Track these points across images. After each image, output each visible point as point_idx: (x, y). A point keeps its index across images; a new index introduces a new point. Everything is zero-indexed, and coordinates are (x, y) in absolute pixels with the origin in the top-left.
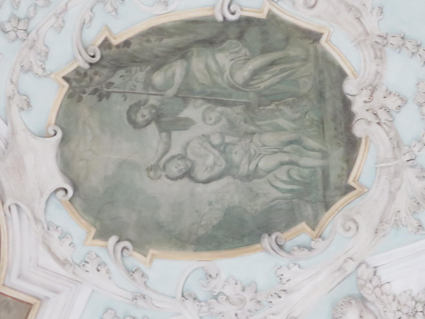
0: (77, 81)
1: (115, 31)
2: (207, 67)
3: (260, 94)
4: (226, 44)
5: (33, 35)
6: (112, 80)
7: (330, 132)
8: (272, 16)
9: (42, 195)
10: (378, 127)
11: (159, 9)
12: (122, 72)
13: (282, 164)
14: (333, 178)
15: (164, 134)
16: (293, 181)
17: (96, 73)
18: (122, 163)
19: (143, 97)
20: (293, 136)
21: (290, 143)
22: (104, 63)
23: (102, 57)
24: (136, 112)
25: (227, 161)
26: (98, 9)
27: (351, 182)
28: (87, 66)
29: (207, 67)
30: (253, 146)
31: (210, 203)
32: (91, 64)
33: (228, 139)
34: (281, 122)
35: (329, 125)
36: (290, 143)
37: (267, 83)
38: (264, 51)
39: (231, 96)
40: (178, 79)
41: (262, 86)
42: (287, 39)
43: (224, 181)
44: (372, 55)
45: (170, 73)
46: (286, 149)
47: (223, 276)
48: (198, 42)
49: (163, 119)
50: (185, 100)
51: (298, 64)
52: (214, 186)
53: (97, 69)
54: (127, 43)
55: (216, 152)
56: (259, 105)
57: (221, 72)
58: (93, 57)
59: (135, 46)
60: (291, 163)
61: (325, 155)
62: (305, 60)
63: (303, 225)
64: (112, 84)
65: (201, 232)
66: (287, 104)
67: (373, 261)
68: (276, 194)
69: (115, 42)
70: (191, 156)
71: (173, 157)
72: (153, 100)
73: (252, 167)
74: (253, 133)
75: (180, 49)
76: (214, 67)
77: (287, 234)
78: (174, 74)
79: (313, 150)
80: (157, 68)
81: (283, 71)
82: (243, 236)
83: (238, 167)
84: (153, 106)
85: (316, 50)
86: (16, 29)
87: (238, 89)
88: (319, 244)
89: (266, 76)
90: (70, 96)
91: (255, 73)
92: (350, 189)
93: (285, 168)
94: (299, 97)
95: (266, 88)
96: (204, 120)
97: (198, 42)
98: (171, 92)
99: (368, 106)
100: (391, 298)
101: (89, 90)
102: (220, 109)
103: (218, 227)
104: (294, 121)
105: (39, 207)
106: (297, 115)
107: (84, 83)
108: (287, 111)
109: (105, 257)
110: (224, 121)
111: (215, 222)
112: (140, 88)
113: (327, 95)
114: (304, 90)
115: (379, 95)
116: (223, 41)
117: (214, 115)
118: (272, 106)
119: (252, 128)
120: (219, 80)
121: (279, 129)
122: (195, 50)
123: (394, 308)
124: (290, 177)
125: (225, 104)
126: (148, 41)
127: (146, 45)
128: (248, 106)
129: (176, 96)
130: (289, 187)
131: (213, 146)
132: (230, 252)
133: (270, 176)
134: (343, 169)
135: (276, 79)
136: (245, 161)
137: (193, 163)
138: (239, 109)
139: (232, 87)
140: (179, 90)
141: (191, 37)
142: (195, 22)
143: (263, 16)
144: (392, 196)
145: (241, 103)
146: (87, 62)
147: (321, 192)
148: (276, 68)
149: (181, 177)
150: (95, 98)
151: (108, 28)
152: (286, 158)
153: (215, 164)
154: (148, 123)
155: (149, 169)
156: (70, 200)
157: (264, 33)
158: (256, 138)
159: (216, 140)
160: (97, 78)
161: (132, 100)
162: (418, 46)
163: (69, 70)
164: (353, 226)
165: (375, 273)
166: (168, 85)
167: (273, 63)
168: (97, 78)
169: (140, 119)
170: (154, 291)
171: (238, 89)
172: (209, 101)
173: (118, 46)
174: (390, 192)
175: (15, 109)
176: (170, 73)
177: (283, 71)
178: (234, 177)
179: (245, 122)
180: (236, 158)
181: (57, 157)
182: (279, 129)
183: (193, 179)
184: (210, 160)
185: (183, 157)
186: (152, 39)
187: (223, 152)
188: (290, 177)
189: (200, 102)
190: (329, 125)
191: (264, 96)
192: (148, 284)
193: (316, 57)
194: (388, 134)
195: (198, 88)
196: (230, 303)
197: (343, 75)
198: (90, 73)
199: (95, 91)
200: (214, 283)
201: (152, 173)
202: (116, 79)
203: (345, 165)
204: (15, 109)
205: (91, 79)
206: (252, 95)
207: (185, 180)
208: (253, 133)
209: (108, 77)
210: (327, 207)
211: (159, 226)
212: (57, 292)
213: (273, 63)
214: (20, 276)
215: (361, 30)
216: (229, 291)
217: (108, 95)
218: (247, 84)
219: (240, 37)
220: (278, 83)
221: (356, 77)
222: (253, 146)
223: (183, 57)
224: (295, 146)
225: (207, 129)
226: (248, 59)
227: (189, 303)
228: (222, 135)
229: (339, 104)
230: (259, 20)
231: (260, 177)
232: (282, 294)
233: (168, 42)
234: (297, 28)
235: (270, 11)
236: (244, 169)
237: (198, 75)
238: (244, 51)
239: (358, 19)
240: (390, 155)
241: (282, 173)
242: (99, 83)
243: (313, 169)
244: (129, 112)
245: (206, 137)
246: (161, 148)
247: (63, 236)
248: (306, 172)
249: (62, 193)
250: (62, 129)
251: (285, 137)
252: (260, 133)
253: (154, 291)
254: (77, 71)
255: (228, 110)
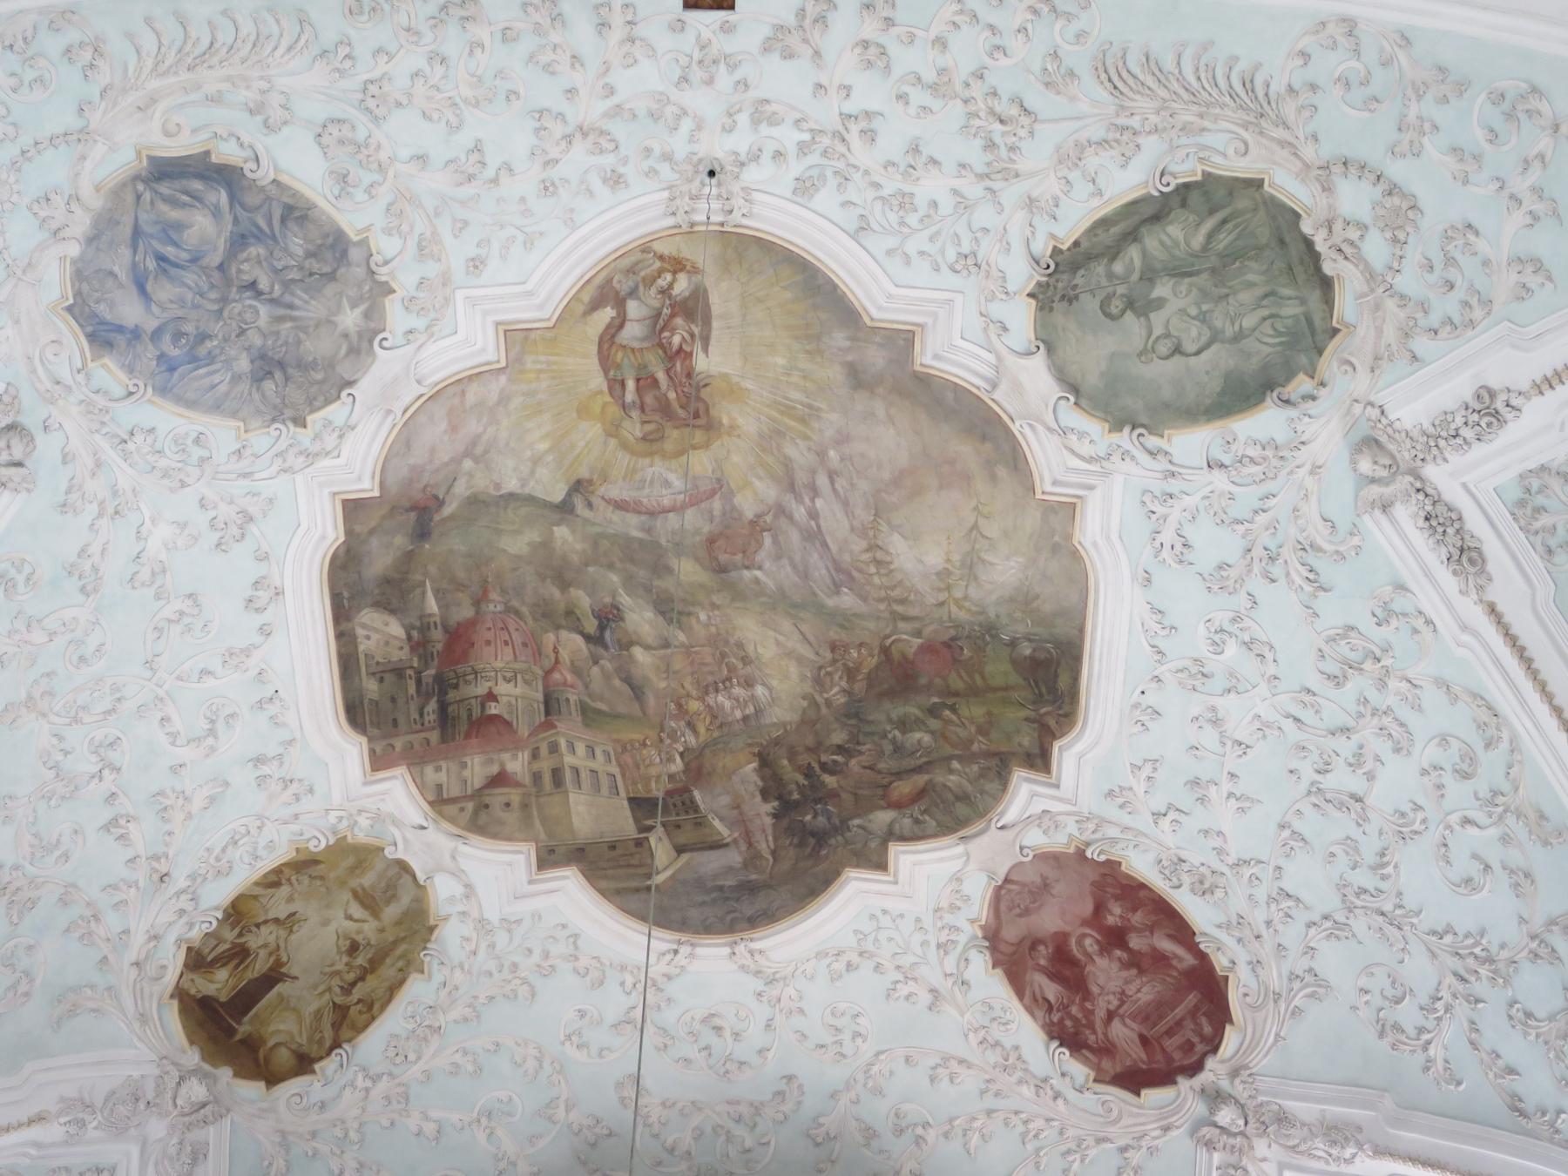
0: (1043, 293)
1: (1060, 234)
2: (1162, 243)
3: (1222, 256)
4: (1172, 216)
5: (984, 266)
6: (1075, 282)
7: (1301, 277)
8: (1206, 175)
9: (1047, 406)
10: (1345, 262)
11: (1096, 202)
12: (1082, 272)
13: (1264, 319)
14: (1318, 322)
15: (1142, 319)
16: (1279, 334)
17: (1057, 281)
18: (1113, 357)
19: (1110, 290)
20: (1266, 289)
21: (1266, 296)
22: (1061, 268)
23: (1057, 265)
24: (1109, 305)
25: (1210, 328)
26: (1037, 221)
27: (1334, 324)
28: (1044, 279)
29: (1162, 243)
30: (1231, 308)
31: (1207, 373)
32: (1049, 275)
33: (1205, 307)
34: (1250, 277)
35: (1298, 270)
36: (1266, 296)
37: (1225, 242)
38: (1212, 212)
39: (1193, 265)
40: (1137, 262)
41: (1221, 246)
42: (1231, 194)
43: (1214, 347)
44: (1319, 188)
45: (1127, 260)
46: (1264, 302)
47: (1242, 438)
48: (1144, 222)
49: (1137, 305)
50: (1151, 281)
51: (1248, 216)
52: (1205, 356)
53: (1057, 276)
54: (1076, 244)
55: (1196, 322)
56: (1224, 267)
57: (1177, 244)
58: (1048, 267)
59: (1085, 244)
60: (1272, 316)
61: (1303, 301)
62: (1255, 210)
63: (1301, 377)
64: (1076, 286)
65: (1208, 402)
66: (1249, 259)
67: (1378, 399)
68: (1268, 350)
69: (1064, 247)
70: (1174, 333)
71: (1158, 338)
72: (1121, 290)
73: (1237, 327)
74: (1227, 295)
75: (1130, 233)
76: (1168, 242)
77: (1289, 388)
78: (1132, 259)
79: (1290, 298)
80: (1113, 259)
81: (1236, 226)
82: (1248, 398)
83: (1223, 332)
84: (1123, 295)
85: (1262, 196)
86: (966, 267)
87: (1197, 256)
88: (1323, 392)
89: (1222, 236)
90: (1040, 308)
91: (1210, 236)
92: (1335, 331)
93: (1268, 322)
94: (1260, 249)
95: (1225, 248)
96: (1175, 295)
97: (1144, 222)
98: (1135, 277)
99: (1329, 243)
100: (1403, 434)
101: (1057, 298)
102: (1187, 280)
103: (1223, 393)
104: (1264, 273)
105: (1049, 418)
106: (1264, 267)
107: (1050, 293)
108: (1252, 264)
109: (1127, 445)
110: (1195, 291)
111: (1218, 389)
112: (1104, 282)
113: (1287, 239)
114: (1264, 241)
115: (1338, 227)
116: (1168, 214)
117: (1183, 288)
118: (1237, 264)
119: (1226, 291)
120: (1177, 253)
121: (1251, 285)
122: (1144, 230)
123: (1409, 446)
124: (1275, 330)
125: (1190, 274)
126: (1096, 235)
127: (1094, 240)
128: (1213, 271)
129: (1141, 279)
130: (1277, 340)
131: (1193, 318)
132: (1240, 416)
133: (1257, 332)
134: (1324, 311)
135: (1231, 238)
136: (1228, 323)
137: (1178, 338)
138: (1205, 276)
139: (1192, 255)
140: (1143, 273)
141: (1136, 219)
142: (1134, 203)
143: (1199, 177)
144: (1379, 331)
145: (1206, 270)
146: (1044, 275)
147: (1310, 339)
148: (1229, 226)
149: (1172, 355)
150: (1065, 304)
151: (1053, 236)
152: (1266, 312)
153: (1200, 334)
154: (1123, 312)
155: (1140, 355)
156: (1075, 404)
157: (1206, 193)
158: (1231, 299)
159: (1193, 311)
160: (1060, 285)
161: (1101, 295)
162: (1363, 167)
163: (1030, 288)
164: (1349, 369)
165: (1383, 413)
166: (1130, 269)
167: (1224, 222)
168: (1060, 285)
169: (1114, 311)
170: (1182, 466)
171: (1197, 256)
172: (1174, 276)
173: (1069, 249)
174: (1376, 327)
175: (994, 338)
176: (1127, 260)
177: (1236, 226)
178: (1223, 342)
179: (1216, 286)
180: (1218, 324)
181: (1050, 369)
182: (1251, 285)
183: (1182, 353)
184: (1194, 332)
185: (1167, 335)
186: (1099, 231)
187: (1203, 321)
188: (1275, 330)
189: (1167, 278)
190: (1298, 270)
191: (1227, 256)
192: (1175, 461)
193: (1265, 203)
194: (1356, 266)
195: (1158, 266)
196: (334, 1099)
197: (1298, 216)
198: (1052, 281)
199: (1063, 297)
200: (1234, 447)
201: (1143, 358)
202: (1079, 280)
203: (1325, 307)
204: (994, 338)
205: (1055, 288)
206: (1213, 258)
207: (1177, 358)
208: (1227, 295)
209: (1070, 281)
210: (1320, 352)
211: (1167, 406)
212: (1091, 488)
213: (1224, 222)
214: (1055, 483)
215: (1299, 164)
216: (1251, 452)
217: (1077, 297)
218: (1206, 248)
219: (1184, 204)
220: (1235, 240)
221: (1309, 215)
222: (1231, 308)
223: (1135, 240)
224: (1271, 298)
225: (1181, 303)
226: (1198, 224)
227: (1216, 472)
228: (1198, 305)
229: (1302, 247)
230: (1196, 182)
231: (1247, 337)
232: (1301, 446)
233: (1115, 230)
234: (1237, 179)
235: (1203, 171)
236: (1229, 332)
237: (1156, 253)
238: (1192, 218)
239: (1295, 154)
240: (1365, 288)
241: (1267, 328)
242: (1064, 289)
243: (1295, 316)
244: (1101, 307)
245: (1183, 311)
246: (1144, 334)
247: (1082, 435)
248: (1289, 322)
249: (1062, 402)
250: (1043, 341)
251: (1259, 291)
252: (1235, 294)
253: (1182, 466)
254: (1039, 284)
255: (1194, 279)
